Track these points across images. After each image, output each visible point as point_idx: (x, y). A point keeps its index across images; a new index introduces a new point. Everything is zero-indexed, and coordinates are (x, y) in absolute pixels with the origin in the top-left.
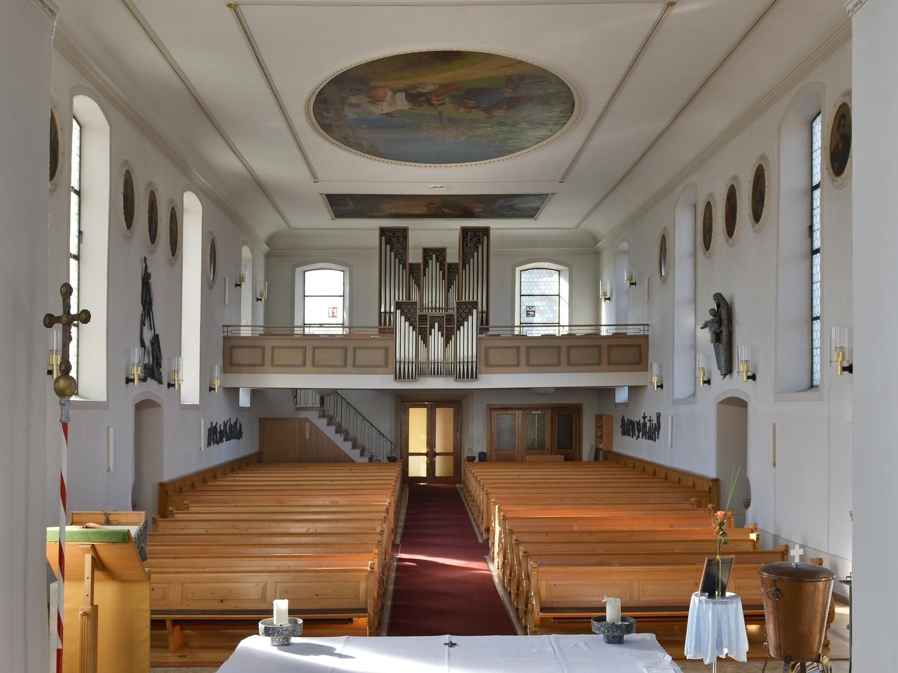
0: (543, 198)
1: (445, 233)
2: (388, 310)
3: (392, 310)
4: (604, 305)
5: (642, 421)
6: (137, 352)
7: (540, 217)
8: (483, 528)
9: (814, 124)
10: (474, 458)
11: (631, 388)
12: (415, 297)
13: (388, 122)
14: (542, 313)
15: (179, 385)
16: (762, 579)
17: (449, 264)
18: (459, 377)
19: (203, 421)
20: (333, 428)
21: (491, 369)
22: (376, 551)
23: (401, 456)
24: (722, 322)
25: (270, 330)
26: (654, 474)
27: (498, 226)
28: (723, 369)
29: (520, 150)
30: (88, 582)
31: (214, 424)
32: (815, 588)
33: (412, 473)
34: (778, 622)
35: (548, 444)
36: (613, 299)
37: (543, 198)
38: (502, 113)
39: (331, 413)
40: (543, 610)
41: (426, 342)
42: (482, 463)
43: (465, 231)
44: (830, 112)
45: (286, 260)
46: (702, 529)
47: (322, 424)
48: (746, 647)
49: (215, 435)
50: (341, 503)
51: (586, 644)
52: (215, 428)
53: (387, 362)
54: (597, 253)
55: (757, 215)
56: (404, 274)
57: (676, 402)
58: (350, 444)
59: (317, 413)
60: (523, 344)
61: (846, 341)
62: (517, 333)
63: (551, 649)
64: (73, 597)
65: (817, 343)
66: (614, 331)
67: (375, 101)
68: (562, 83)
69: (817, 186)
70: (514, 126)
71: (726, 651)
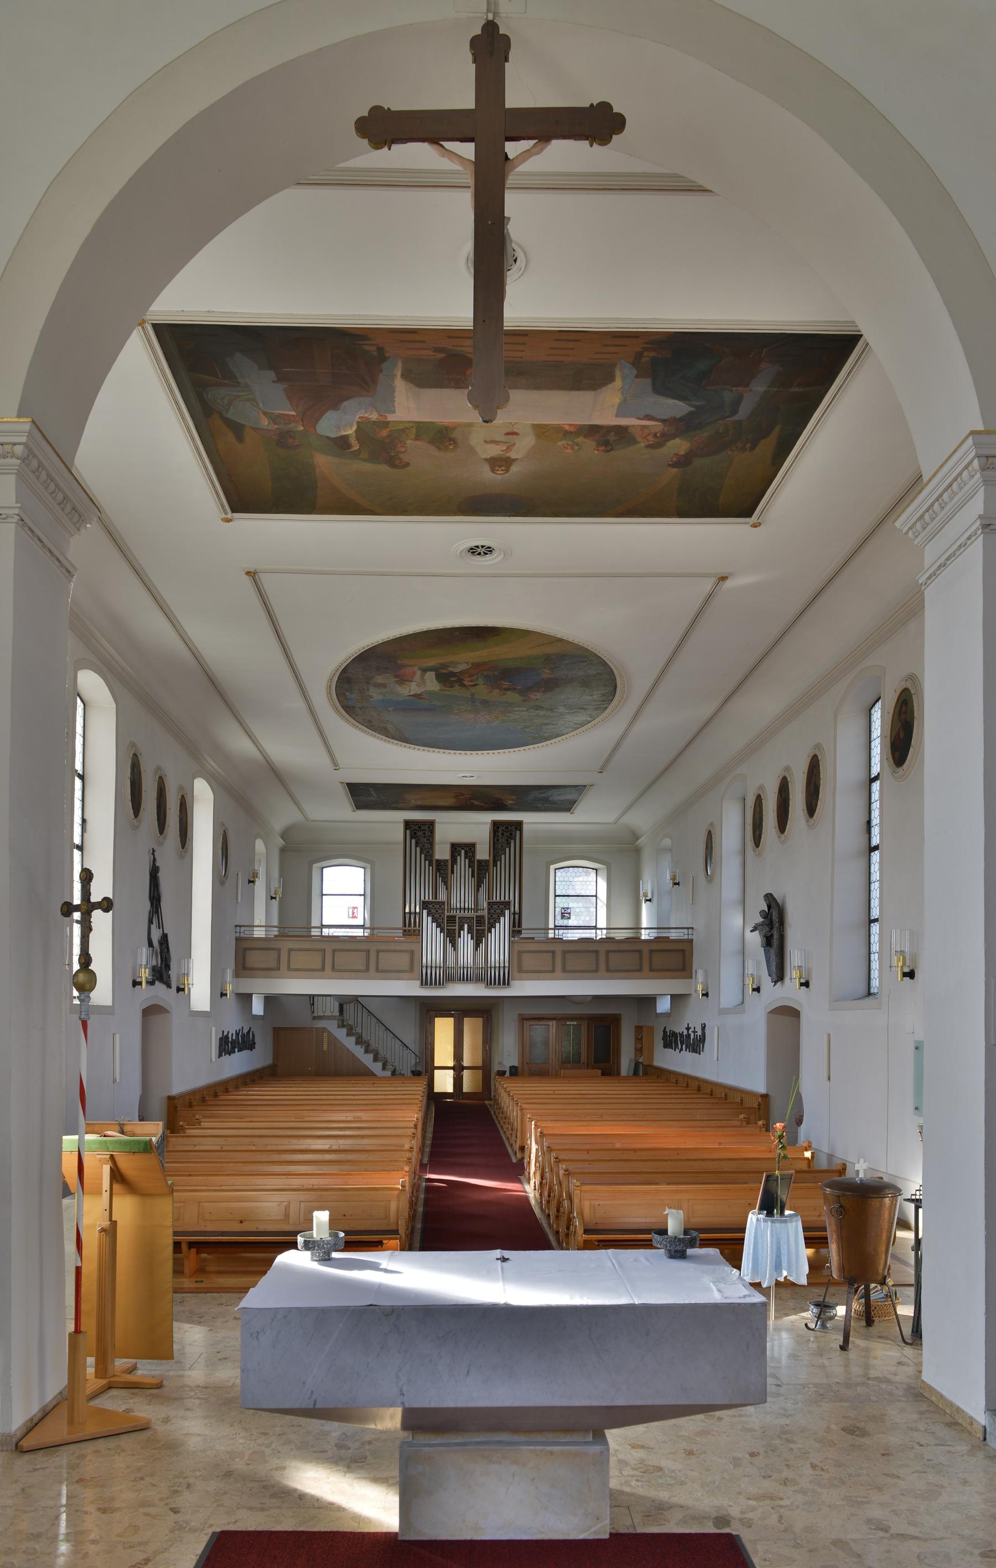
0: (580, 789)
1: (474, 827)
2: (413, 910)
3: (418, 910)
4: (645, 907)
5: (685, 1033)
6: (144, 952)
7: (576, 811)
8: (517, 1147)
9: (873, 711)
10: (504, 1073)
11: (674, 997)
12: (442, 897)
13: (416, 705)
14: (578, 915)
15: (189, 989)
16: (825, 1195)
17: (479, 861)
18: (490, 983)
19: (214, 1029)
20: (353, 1039)
21: (525, 975)
22: (407, 1168)
23: (426, 1069)
24: (773, 925)
25: (286, 931)
26: (699, 1089)
27: (531, 820)
28: (774, 975)
29: (557, 737)
30: (106, 1195)
31: (225, 1033)
32: (881, 1205)
33: (438, 1088)
34: (842, 1241)
35: (584, 1058)
36: (655, 900)
37: (580, 789)
38: (539, 695)
39: (351, 1022)
40: (586, 1231)
41: (454, 945)
42: (514, 1078)
43: (496, 825)
44: (891, 698)
45: (302, 856)
46: (750, 1151)
47: (341, 1034)
48: (806, 1269)
49: (227, 1046)
50: (364, 1118)
51: (647, 1259)
52: (227, 1037)
53: (413, 967)
54: (637, 851)
55: (811, 809)
56: (430, 871)
57: (723, 1012)
58: (371, 1056)
59: (335, 1023)
60: (559, 948)
61: (907, 944)
62: (551, 935)
63: (610, 1264)
64: (91, 1212)
65: (875, 947)
66: (656, 935)
67: (402, 680)
68: (604, 664)
69: (876, 778)
70: (551, 710)
71: (785, 1273)
